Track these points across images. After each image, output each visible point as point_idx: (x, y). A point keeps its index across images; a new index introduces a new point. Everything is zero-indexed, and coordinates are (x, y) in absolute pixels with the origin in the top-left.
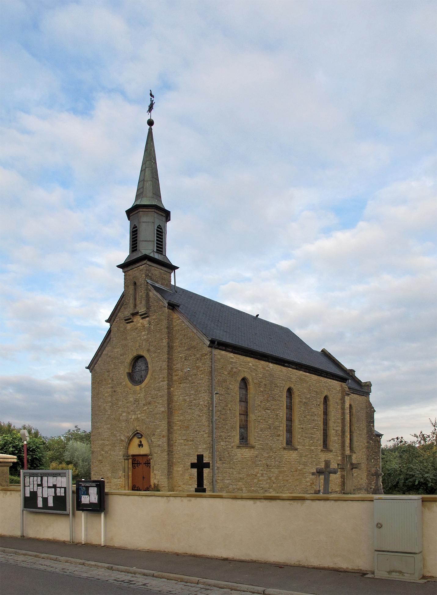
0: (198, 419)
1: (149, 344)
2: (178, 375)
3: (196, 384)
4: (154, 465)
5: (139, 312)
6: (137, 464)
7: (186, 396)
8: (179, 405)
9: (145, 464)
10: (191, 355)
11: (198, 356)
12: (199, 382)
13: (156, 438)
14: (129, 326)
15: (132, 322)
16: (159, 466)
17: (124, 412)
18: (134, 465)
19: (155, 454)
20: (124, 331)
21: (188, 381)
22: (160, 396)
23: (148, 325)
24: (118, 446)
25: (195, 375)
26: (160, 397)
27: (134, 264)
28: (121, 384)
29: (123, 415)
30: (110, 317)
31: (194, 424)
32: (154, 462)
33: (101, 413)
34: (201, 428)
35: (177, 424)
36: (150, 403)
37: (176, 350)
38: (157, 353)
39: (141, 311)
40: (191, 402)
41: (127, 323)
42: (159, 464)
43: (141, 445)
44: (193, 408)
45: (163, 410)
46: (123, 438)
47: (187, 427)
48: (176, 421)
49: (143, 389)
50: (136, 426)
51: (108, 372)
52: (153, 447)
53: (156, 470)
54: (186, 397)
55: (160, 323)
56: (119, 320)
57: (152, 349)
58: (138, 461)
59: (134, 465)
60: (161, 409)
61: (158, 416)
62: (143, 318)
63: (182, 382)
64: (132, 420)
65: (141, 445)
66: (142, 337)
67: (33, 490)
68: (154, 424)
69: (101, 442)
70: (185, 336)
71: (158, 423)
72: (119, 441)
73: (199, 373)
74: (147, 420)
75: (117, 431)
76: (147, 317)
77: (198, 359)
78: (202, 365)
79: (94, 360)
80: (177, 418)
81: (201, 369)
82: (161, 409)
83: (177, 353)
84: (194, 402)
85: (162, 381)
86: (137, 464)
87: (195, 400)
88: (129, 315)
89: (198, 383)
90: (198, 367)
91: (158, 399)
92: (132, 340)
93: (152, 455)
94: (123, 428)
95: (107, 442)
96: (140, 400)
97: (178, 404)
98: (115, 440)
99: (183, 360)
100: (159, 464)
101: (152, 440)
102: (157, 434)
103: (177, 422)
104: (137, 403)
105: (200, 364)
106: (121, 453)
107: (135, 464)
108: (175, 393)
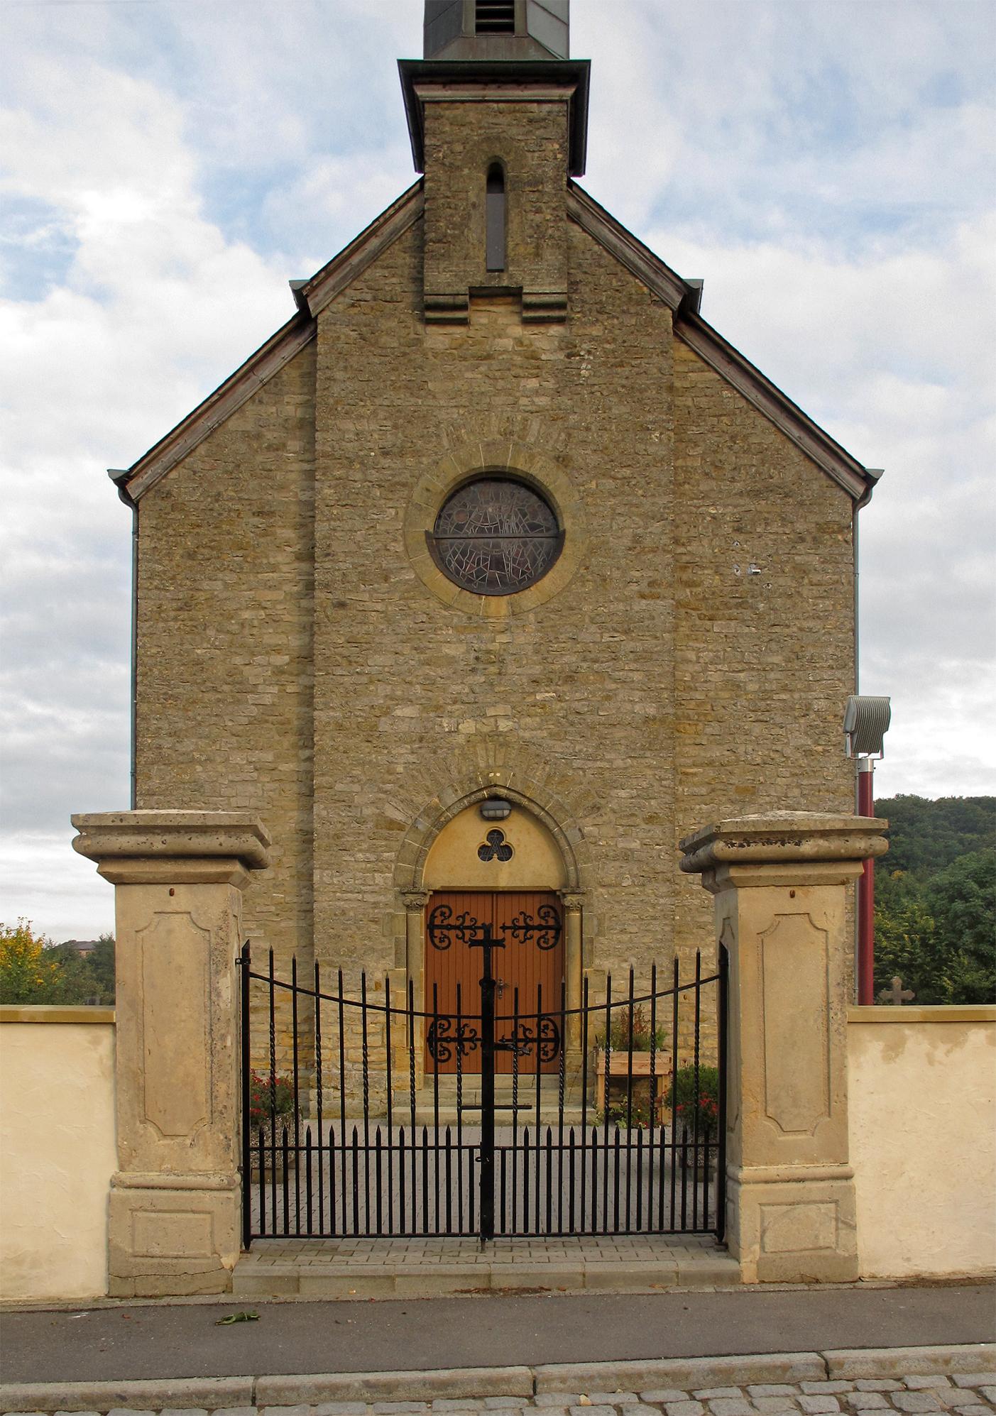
0: (804, 762)
1: (569, 435)
2: (699, 585)
3: (795, 629)
4: (597, 935)
5: (524, 291)
6: (528, 928)
7: (739, 671)
8: (701, 703)
10: (766, 519)
11: (800, 527)
12: (806, 624)
13: (604, 823)
14: (437, 338)
15: (463, 322)
18: (437, 932)
19: (601, 890)
20: (405, 354)
21: (748, 614)
22: (631, 656)
23: (561, 356)
24: (365, 846)
25: (790, 596)
26: (636, 661)
27: (494, 82)
28: (386, 579)
29: (398, 712)
30: (323, 274)
32: (595, 922)
33: (212, 696)
34: (815, 800)
35: (695, 774)
36: (570, 679)
37: (687, 486)
38: (615, 478)
39: (536, 289)
40: (766, 695)
41: (429, 322)
43: (496, 848)
44: (779, 719)
46: (399, 816)
47: (746, 790)
48: (689, 761)
50: (488, 766)
51: (259, 514)
52: (588, 859)
53: (610, 955)
54: (742, 675)
55: (634, 363)
56: (375, 299)
57: (581, 455)
59: (437, 932)
60: (637, 708)
61: (619, 733)
62: (527, 322)
63: (720, 613)
64: (461, 739)
66: (524, 401)
67: (626, 1071)
68: (599, 764)
70: (733, 438)
72: (370, 825)
73: (805, 592)
74: (558, 746)
75: (355, 780)
76: (560, 321)
78: (823, 563)
79: (170, 444)
80: (693, 751)
81: (816, 578)
82: (637, 708)
83: (692, 499)
84: (783, 696)
85: (643, 597)
87: (785, 689)
88: (463, 288)
89: (801, 629)
90: (802, 571)
92: (464, 401)
94: (400, 769)
96: (509, 658)
97: (698, 696)
98: (346, 820)
99: (727, 529)
100: (623, 931)
101: (586, 830)
102: (615, 807)
103: (695, 765)
104: (493, 669)
105: (815, 561)
107: (450, 927)
108: (681, 650)
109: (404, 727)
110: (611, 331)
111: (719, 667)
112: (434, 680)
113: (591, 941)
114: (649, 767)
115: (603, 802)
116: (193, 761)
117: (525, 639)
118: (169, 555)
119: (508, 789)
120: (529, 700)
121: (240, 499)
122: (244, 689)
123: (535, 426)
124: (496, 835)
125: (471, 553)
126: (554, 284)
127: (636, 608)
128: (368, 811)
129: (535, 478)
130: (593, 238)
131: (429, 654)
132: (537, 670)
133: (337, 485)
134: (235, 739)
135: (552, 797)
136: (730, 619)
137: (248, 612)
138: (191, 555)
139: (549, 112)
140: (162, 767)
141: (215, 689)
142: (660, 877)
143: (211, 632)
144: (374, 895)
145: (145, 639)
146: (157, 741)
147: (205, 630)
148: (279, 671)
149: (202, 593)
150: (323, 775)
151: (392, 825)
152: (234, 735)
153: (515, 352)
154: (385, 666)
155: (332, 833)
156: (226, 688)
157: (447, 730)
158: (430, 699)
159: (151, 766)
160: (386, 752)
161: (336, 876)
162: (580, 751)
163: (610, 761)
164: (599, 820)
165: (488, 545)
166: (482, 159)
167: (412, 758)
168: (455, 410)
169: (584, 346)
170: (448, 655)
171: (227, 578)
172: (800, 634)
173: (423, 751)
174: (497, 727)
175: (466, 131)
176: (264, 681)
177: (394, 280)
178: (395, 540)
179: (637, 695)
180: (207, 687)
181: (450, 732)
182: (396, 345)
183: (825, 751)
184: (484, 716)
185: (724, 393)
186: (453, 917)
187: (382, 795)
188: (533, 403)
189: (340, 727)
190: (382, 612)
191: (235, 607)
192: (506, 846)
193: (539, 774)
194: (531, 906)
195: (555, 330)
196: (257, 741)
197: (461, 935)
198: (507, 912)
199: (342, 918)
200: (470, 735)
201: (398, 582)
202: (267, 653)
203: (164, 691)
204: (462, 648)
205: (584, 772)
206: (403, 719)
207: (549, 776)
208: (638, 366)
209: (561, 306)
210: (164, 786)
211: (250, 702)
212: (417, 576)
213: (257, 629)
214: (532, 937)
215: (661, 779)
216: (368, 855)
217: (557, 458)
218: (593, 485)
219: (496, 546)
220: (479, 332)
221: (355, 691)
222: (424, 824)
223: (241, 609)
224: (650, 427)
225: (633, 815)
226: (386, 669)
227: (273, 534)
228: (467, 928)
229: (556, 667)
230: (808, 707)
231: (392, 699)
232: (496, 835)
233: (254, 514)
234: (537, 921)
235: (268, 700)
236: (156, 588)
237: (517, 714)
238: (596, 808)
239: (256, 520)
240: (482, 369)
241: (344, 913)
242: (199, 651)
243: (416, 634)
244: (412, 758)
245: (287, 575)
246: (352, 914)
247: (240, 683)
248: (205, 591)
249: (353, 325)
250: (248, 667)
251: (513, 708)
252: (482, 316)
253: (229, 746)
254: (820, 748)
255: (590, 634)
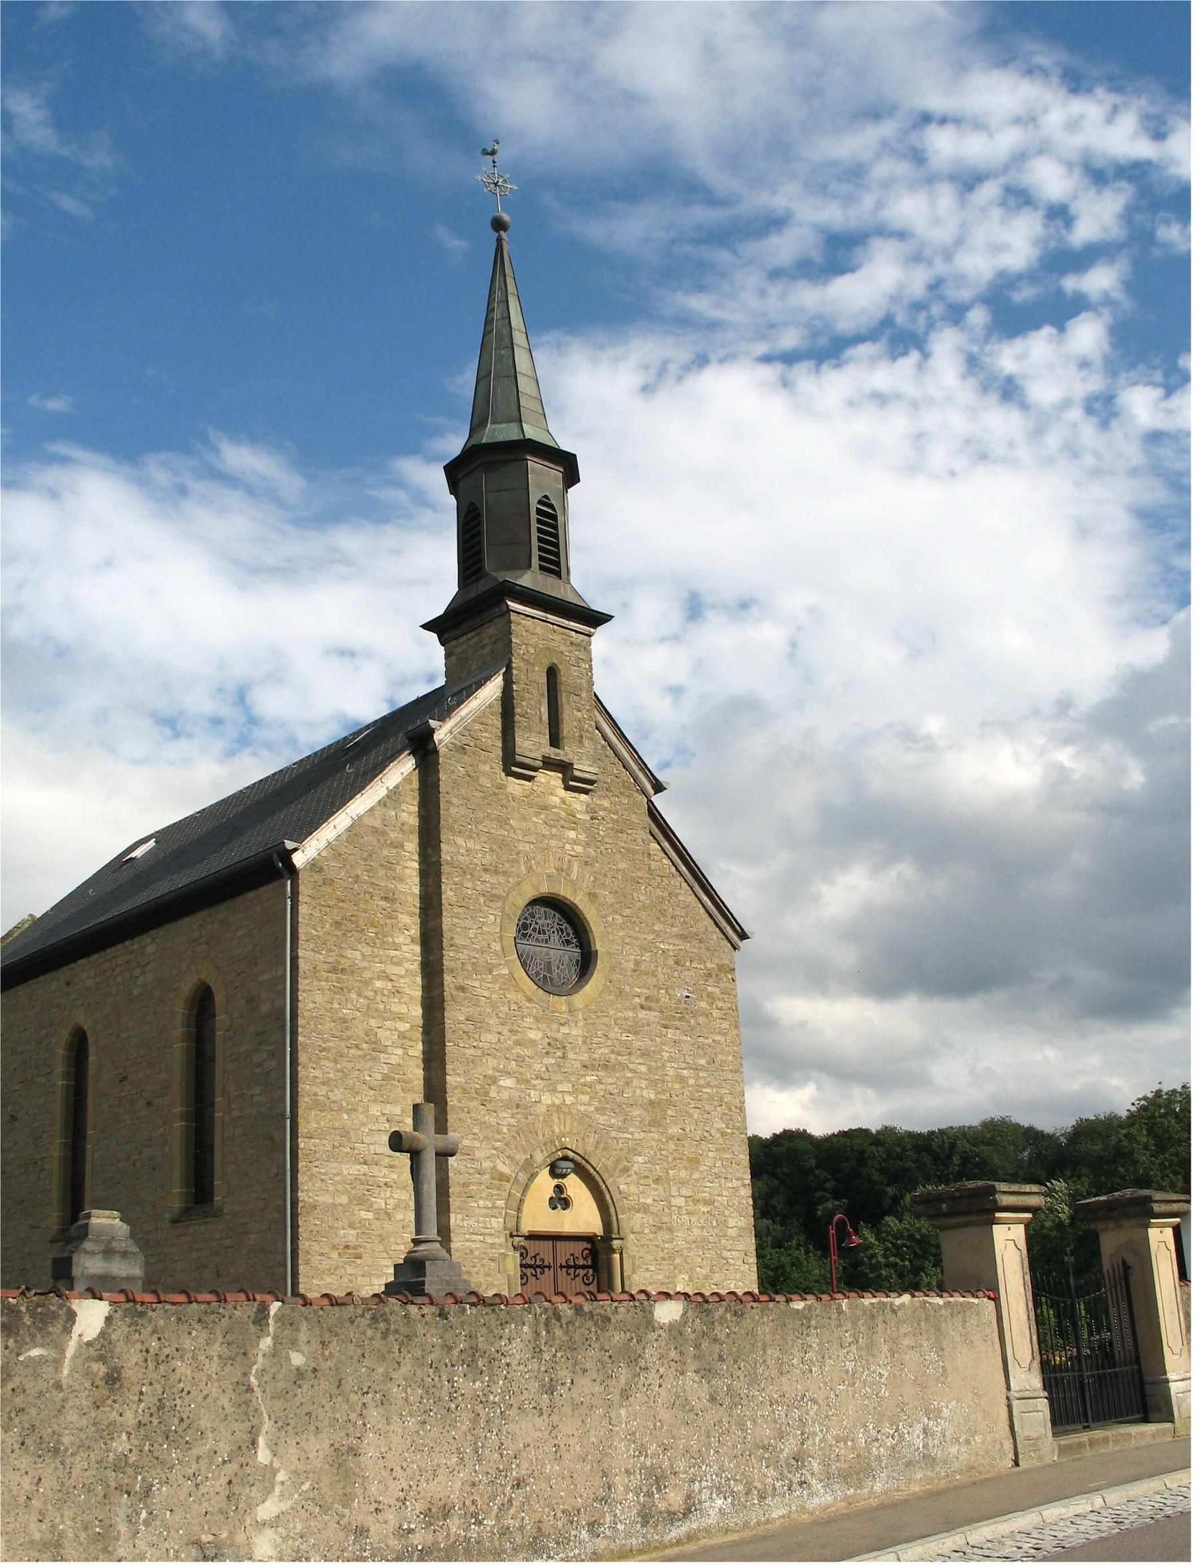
1: (596, 878)
6: (576, 1267)
7: (683, 1069)
9: (564, 1270)
14: (515, 786)
15: (530, 779)
16: (648, 1275)
17: (508, 1074)
24: (484, 1195)
29: (502, 1083)
31: (711, 1154)
42: (647, 1270)
43: (560, 1200)
45: (653, 1097)
46: (505, 1170)
49: (580, 1014)
51: (386, 899)
55: (629, 832)
58: (538, 1258)
62: (568, 788)
65: (560, 1200)
66: (568, 847)
68: (626, 1135)
69: (357, 1169)
71: (637, 1136)
74: (602, 1119)
76: (586, 792)
77: (710, 975)
84: (708, 1090)
86: (576, 1267)
87: (708, 1085)
91: (633, 1059)
92: (533, 839)
93: (622, 1239)
94: (505, 1130)
95: (385, 1171)
98: (471, 1171)
99: (671, 962)
100: (647, 1270)
101: (622, 1187)
106: (497, 1223)
107: (583, 1267)
109: (505, 1095)
110: (615, 806)
111: (673, 1064)
112: (524, 1059)
113: (629, 1277)
114: (653, 1140)
115: (629, 1165)
116: (341, 1109)
117: (576, 1032)
118: (322, 922)
119: (574, 1152)
120: (582, 1080)
121: (372, 883)
122: (378, 1048)
123: (575, 867)
124: (559, 1189)
125: (532, 957)
126: (591, 766)
127: (640, 1016)
128: (487, 1164)
129: (577, 907)
130: (602, 735)
131: (519, 1036)
132: (585, 1057)
133: (456, 889)
134: (372, 1092)
135: (600, 1160)
136: (677, 1029)
137: (380, 982)
138: (337, 924)
139: (582, 641)
140: (318, 1113)
141: (357, 1046)
142: (664, 1226)
143: (353, 996)
144: (492, 1237)
145: (305, 995)
146: (314, 1089)
147: (349, 993)
148: (402, 1036)
149: (346, 960)
150: (454, 1131)
151: (502, 1177)
152: (372, 1089)
153: (560, 808)
154: (491, 1043)
155: (462, 1181)
156: (365, 1046)
157: (534, 1100)
158: (521, 1074)
159: (309, 1111)
160: (495, 1114)
161: (467, 1220)
162: (614, 1124)
163: (632, 1134)
164: (629, 1180)
165: (542, 952)
166: (546, 663)
167: (512, 1121)
168: (527, 844)
169: (600, 813)
170: (531, 1039)
171: (364, 950)
172: (713, 1044)
173: (519, 1116)
174: (564, 1101)
175: (535, 639)
176: (393, 1043)
177: (486, 735)
178: (495, 941)
179: (644, 1084)
180: (351, 1044)
181: (535, 1102)
182: (489, 785)
183: (733, 1133)
184: (555, 1090)
185: (664, 860)
186: (529, 1257)
187: (494, 1152)
188: (573, 850)
189: (464, 1091)
190: (488, 998)
191: (370, 976)
192: (565, 1199)
193: (591, 1140)
194: (578, 1248)
195: (583, 797)
196: (388, 1096)
197: (534, 1273)
198: (565, 1251)
199: (471, 1257)
200: (549, 1106)
201: (497, 975)
202: (394, 1019)
203: (319, 1043)
204: (540, 1035)
205: (617, 1141)
206: (505, 1088)
207: (598, 1142)
208: (631, 835)
209: (592, 782)
210: (320, 1130)
211: (383, 1061)
212: (510, 973)
213: (386, 998)
214: (578, 1275)
215: (660, 1150)
216: (487, 1202)
217: (589, 894)
218: (610, 919)
219: (547, 954)
220: (540, 789)
221: (473, 1062)
222: (523, 1177)
223: (374, 979)
224: (640, 881)
225: (647, 1177)
226: (493, 1046)
227: (396, 918)
228: (572, 1267)
229: (597, 1056)
230: (721, 1099)
231: (497, 1071)
232: (559, 1189)
233: (382, 898)
234: (581, 1262)
235: (394, 1060)
236: (313, 950)
237: (575, 1092)
238: (626, 1170)
239: (383, 903)
240: (542, 816)
241: (471, 1252)
242: (344, 1011)
243: (511, 1019)
244: (512, 1121)
245: (407, 954)
246: (477, 1253)
247: (375, 1043)
248: (348, 958)
249: (462, 763)
250: (380, 1030)
251: (573, 1086)
252: (543, 777)
253: (369, 1098)
254: (729, 1131)
255: (615, 1033)
